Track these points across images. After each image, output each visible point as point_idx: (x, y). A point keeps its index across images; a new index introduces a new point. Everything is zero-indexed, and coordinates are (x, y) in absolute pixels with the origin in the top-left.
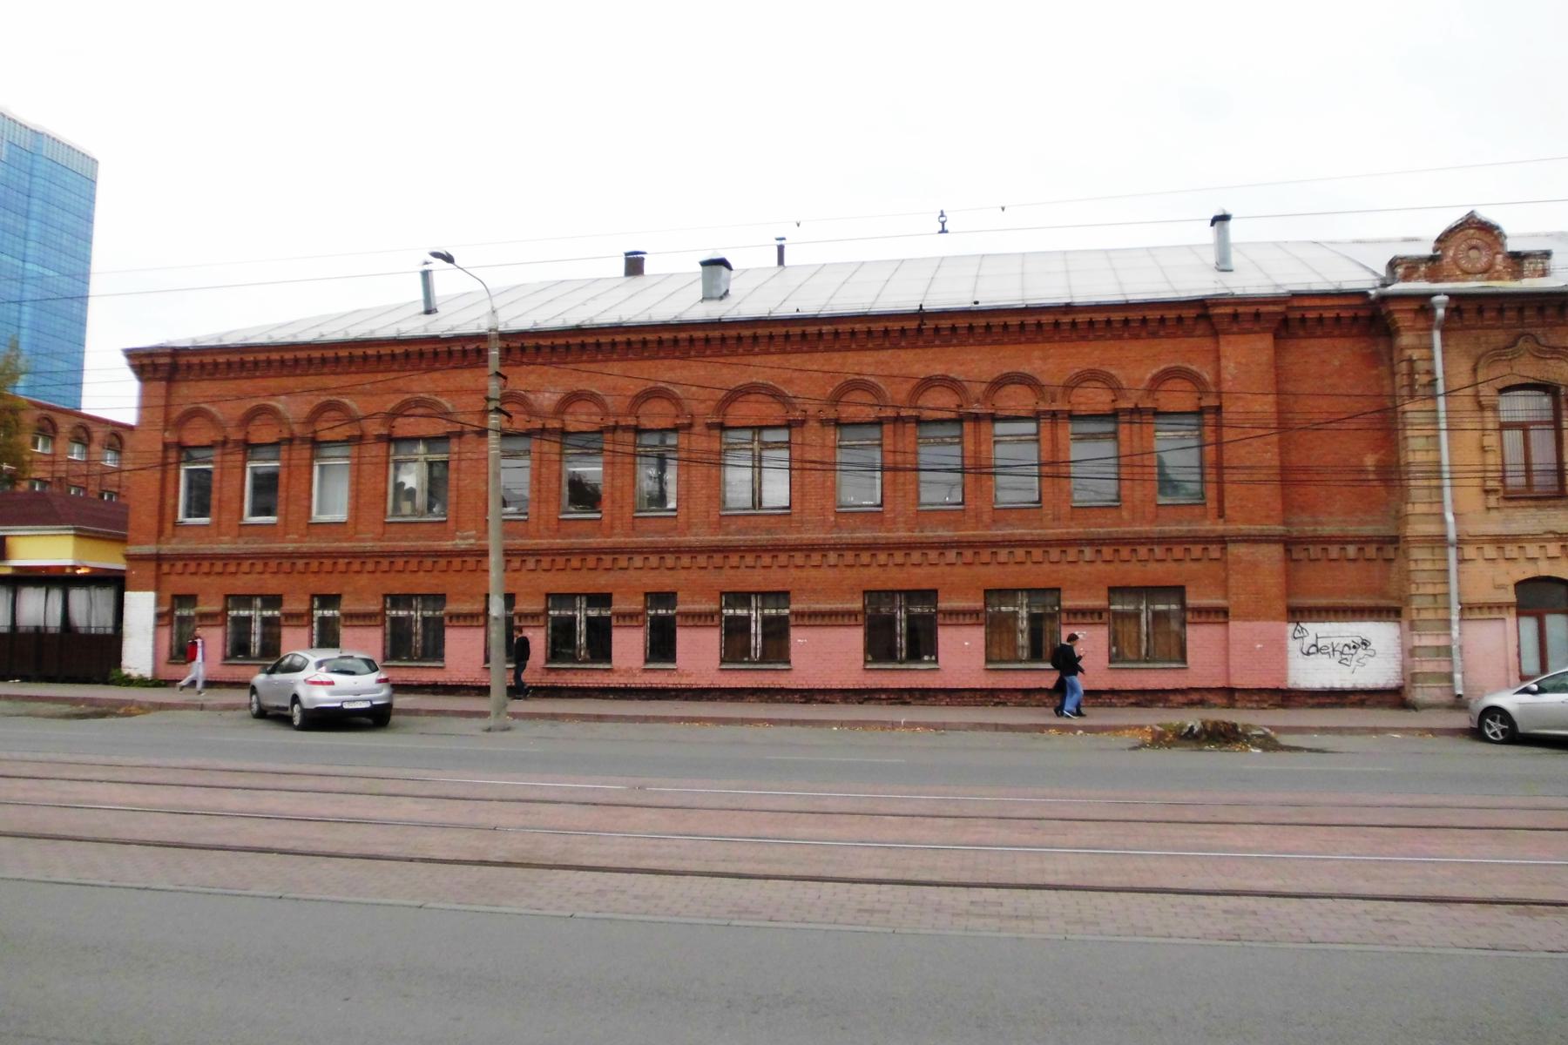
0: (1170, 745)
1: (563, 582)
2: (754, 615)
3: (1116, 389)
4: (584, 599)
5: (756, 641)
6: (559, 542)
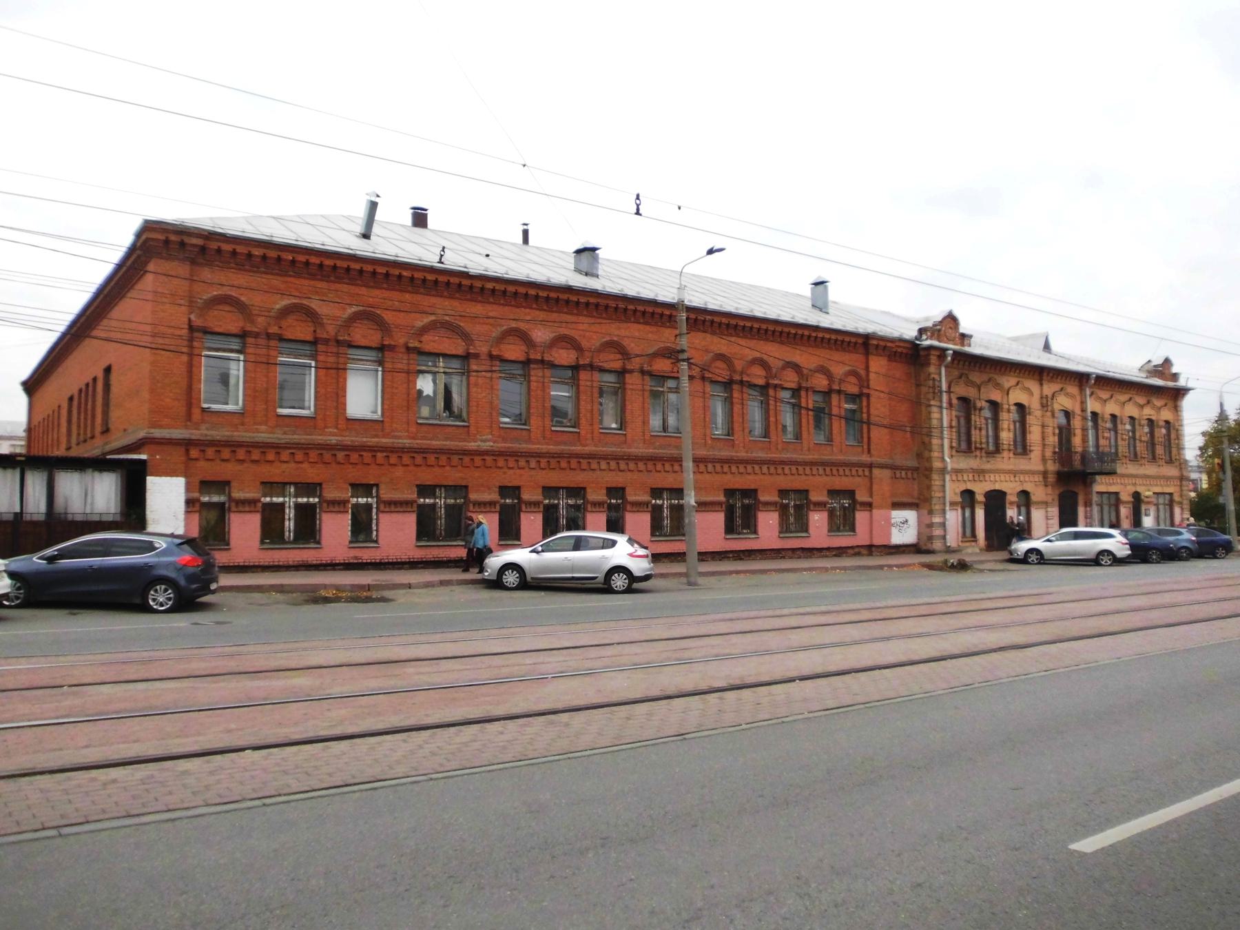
0: (350, 602)
1: (555, 478)
2: (290, 501)
3: (577, 347)
4: (565, 491)
5: (290, 525)
6: (552, 448)
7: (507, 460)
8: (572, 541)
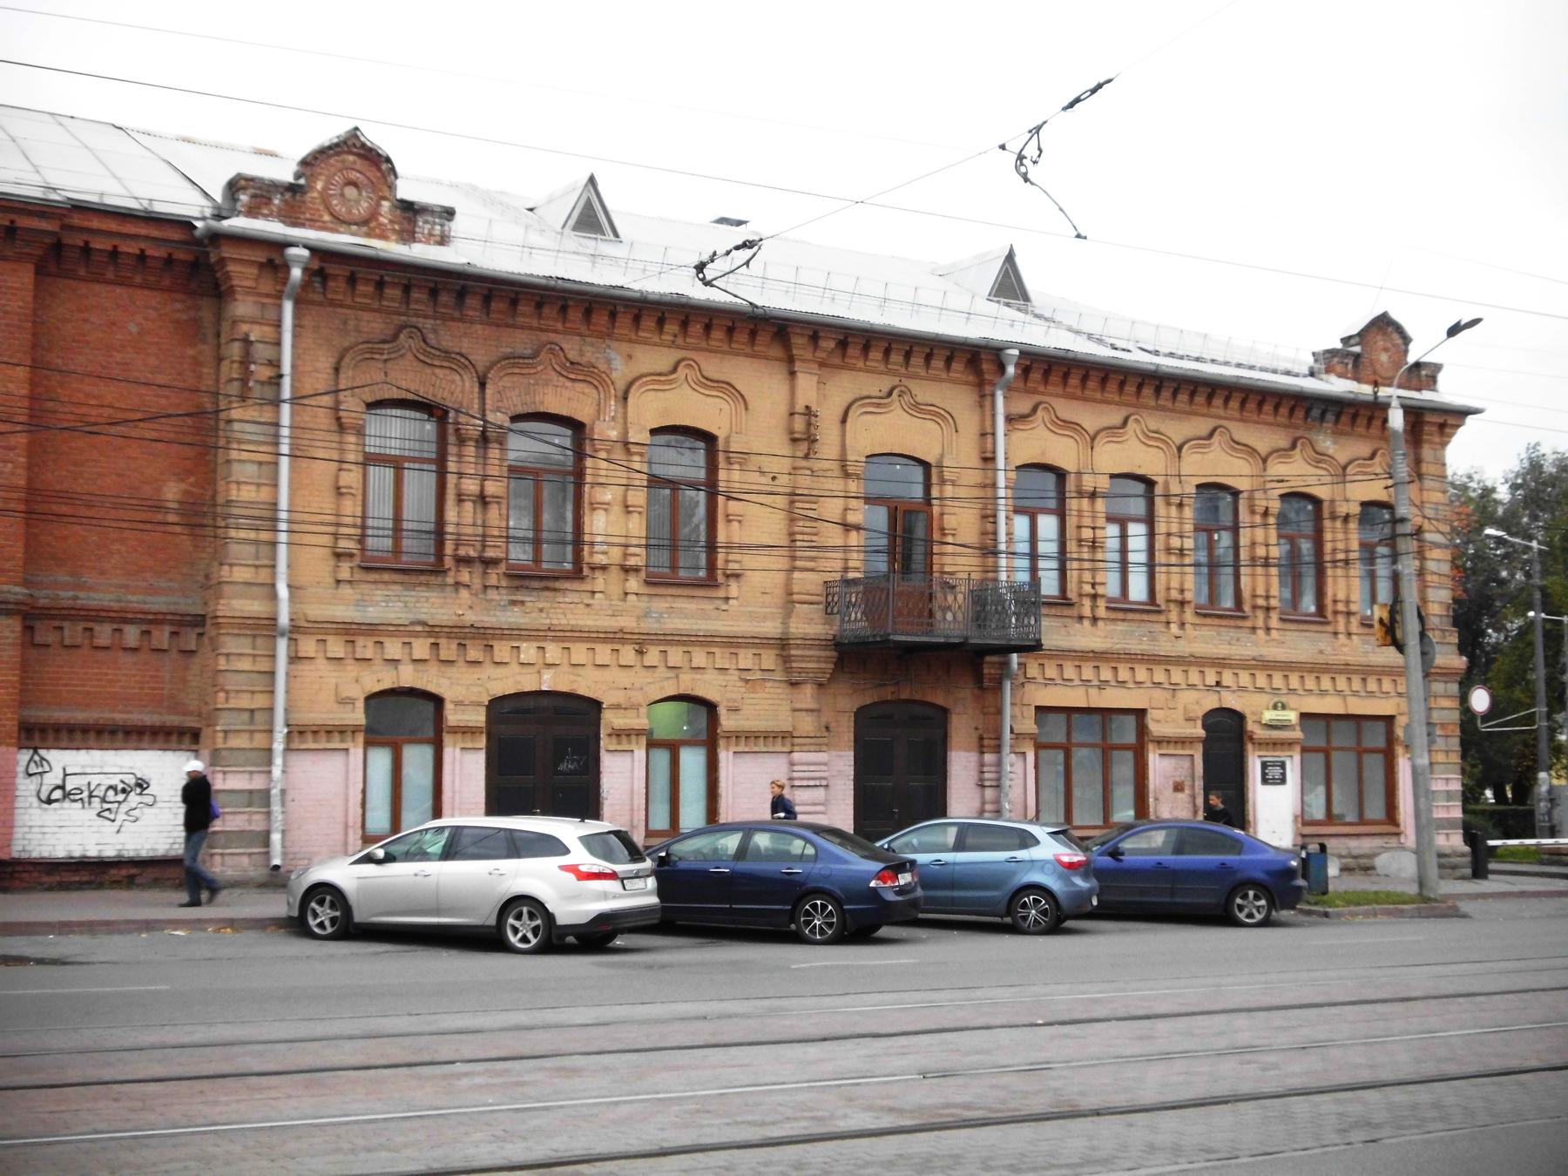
7: (1186, 671)
8: (443, 839)
